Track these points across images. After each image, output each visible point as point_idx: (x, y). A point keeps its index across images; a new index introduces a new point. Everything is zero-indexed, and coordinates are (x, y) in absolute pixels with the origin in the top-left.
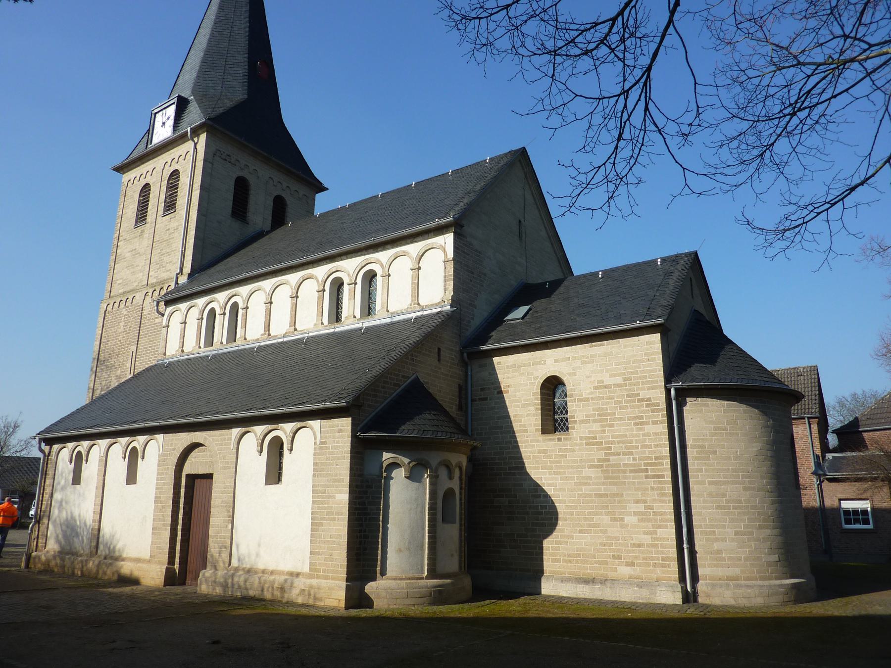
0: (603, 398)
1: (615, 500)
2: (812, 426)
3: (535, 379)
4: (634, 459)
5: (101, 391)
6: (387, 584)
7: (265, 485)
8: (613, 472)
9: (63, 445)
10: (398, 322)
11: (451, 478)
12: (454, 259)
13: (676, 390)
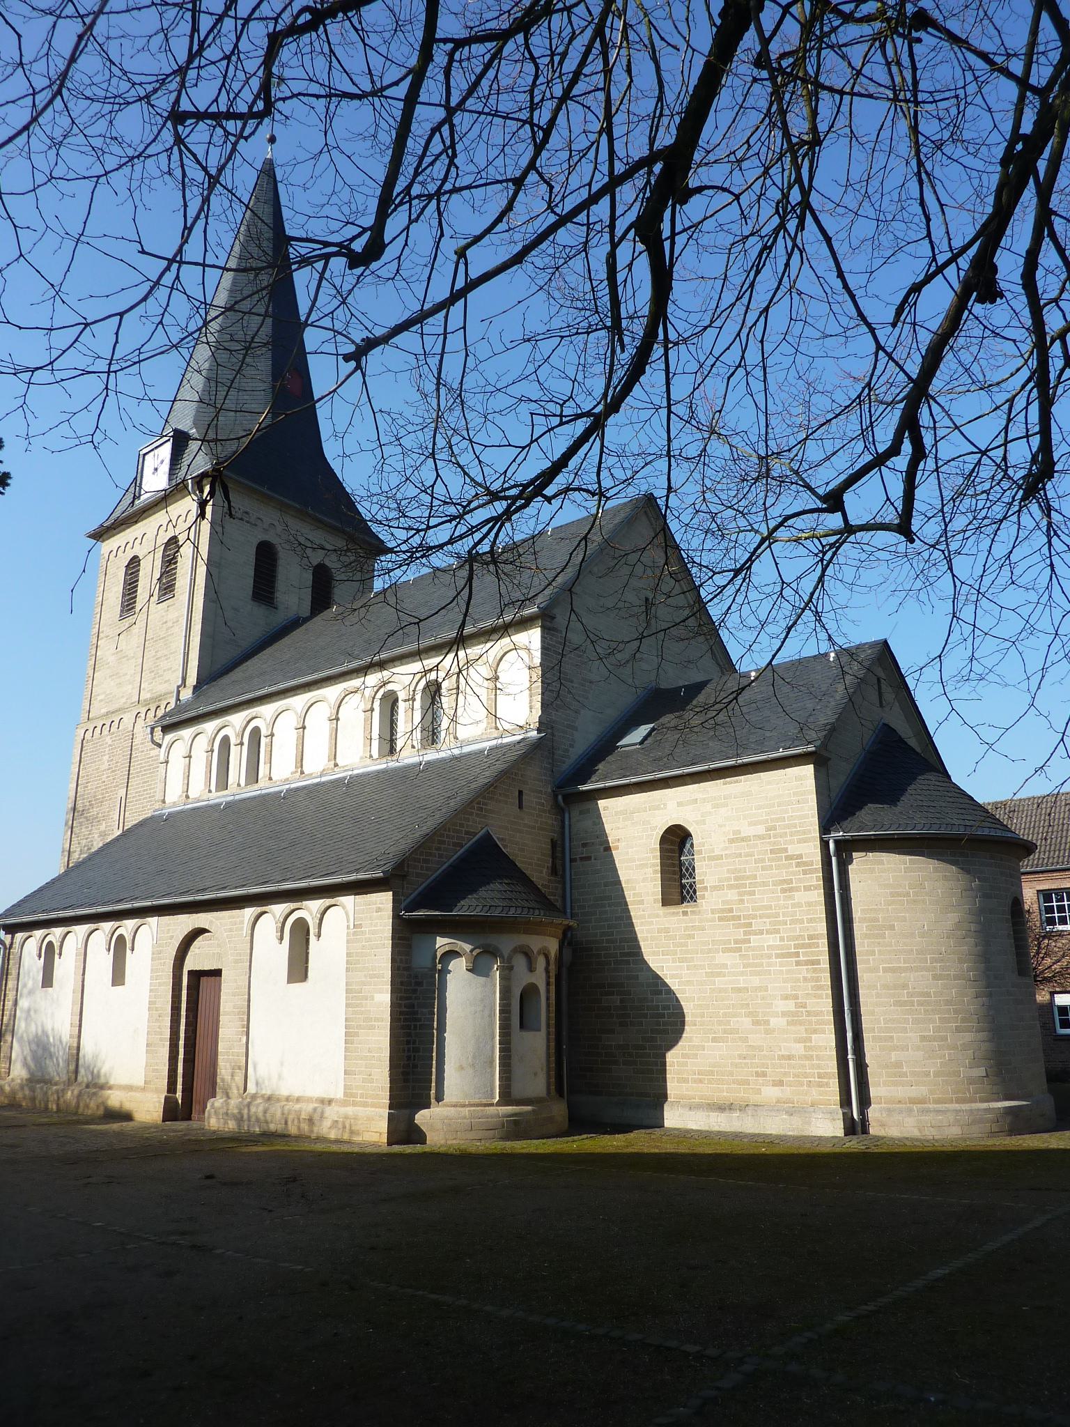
0: (740, 855)
1: (757, 997)
4: (782, 939)
5: (80, 855)
7: (289, 982)
10: (470, 754)
11: (531, 969)
13: (837, 842)
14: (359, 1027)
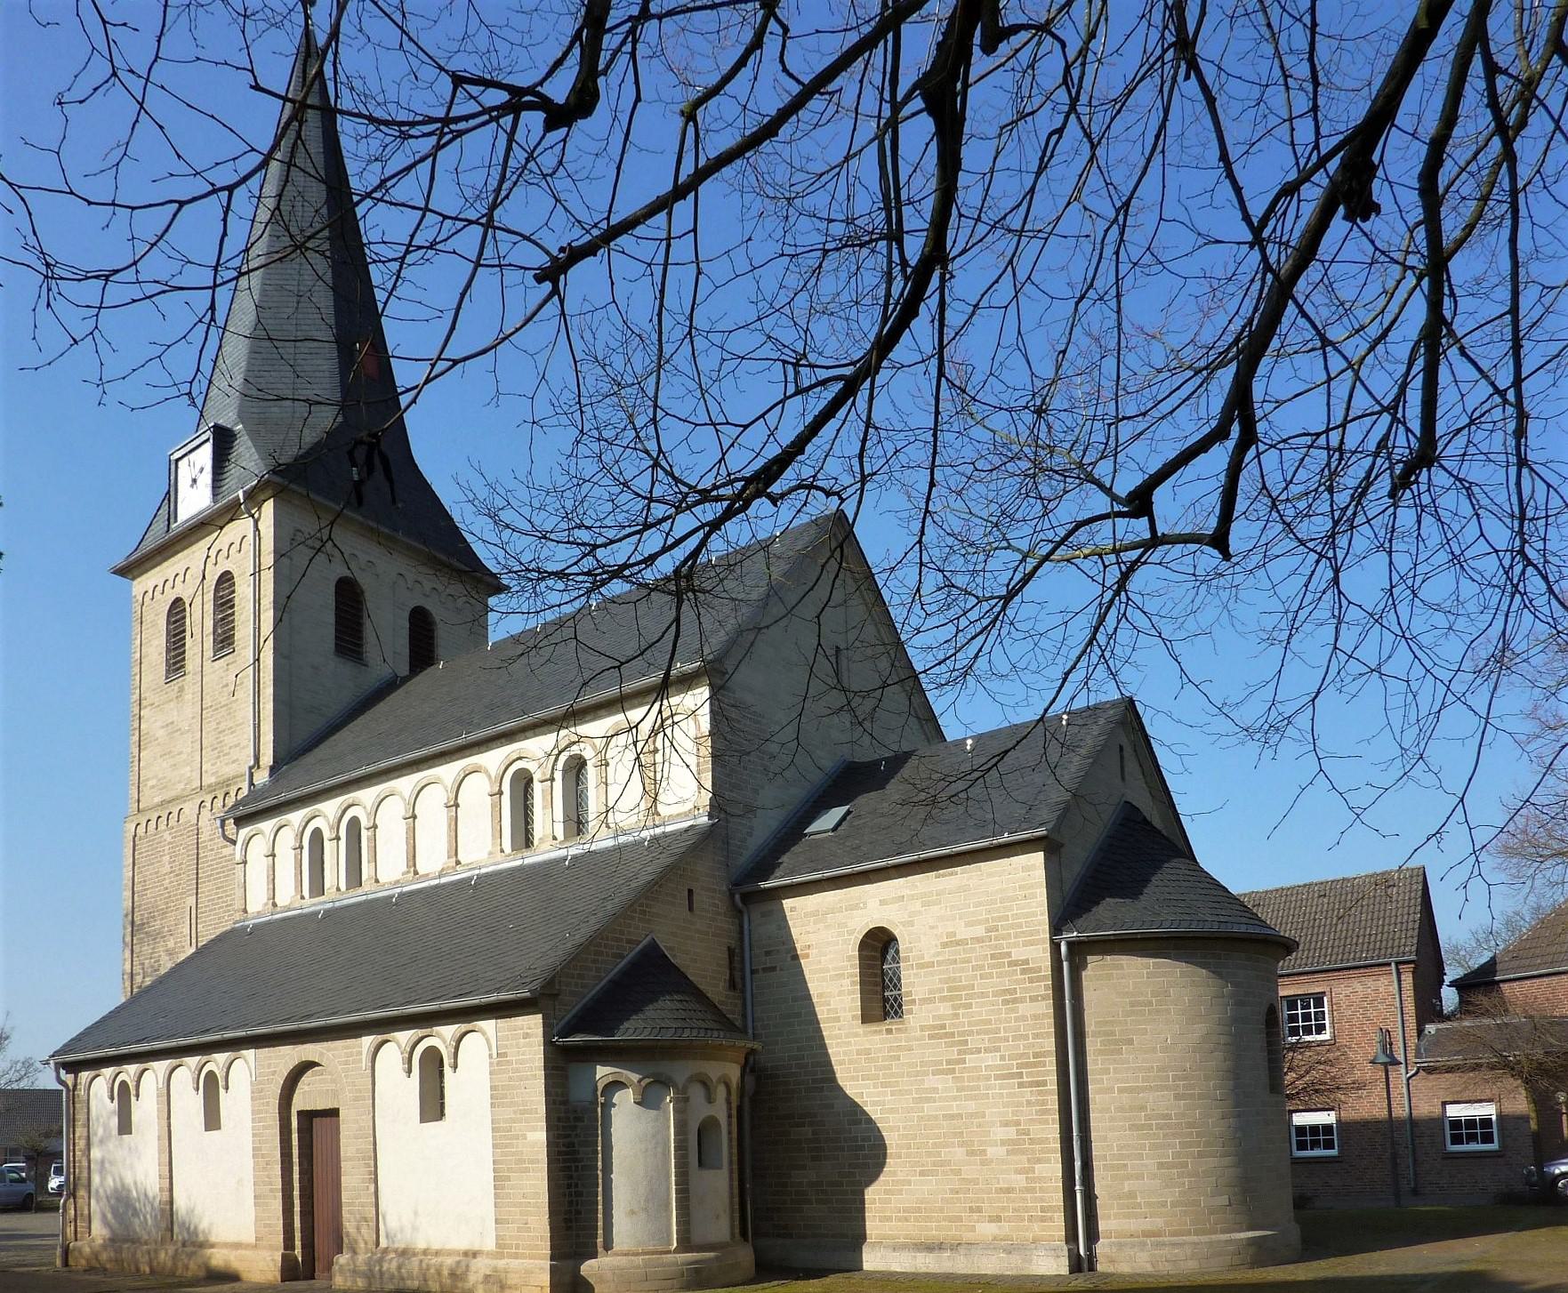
2: (1403, 977)
3: (849, 935)
4: (1003, 1058)
6: (614, 1263)
8: (970, 1079)
9: (97, 1072)
11: (710, 1099)
12: (711, 734)
13: (1070, 944)
14: (510, 1170)
